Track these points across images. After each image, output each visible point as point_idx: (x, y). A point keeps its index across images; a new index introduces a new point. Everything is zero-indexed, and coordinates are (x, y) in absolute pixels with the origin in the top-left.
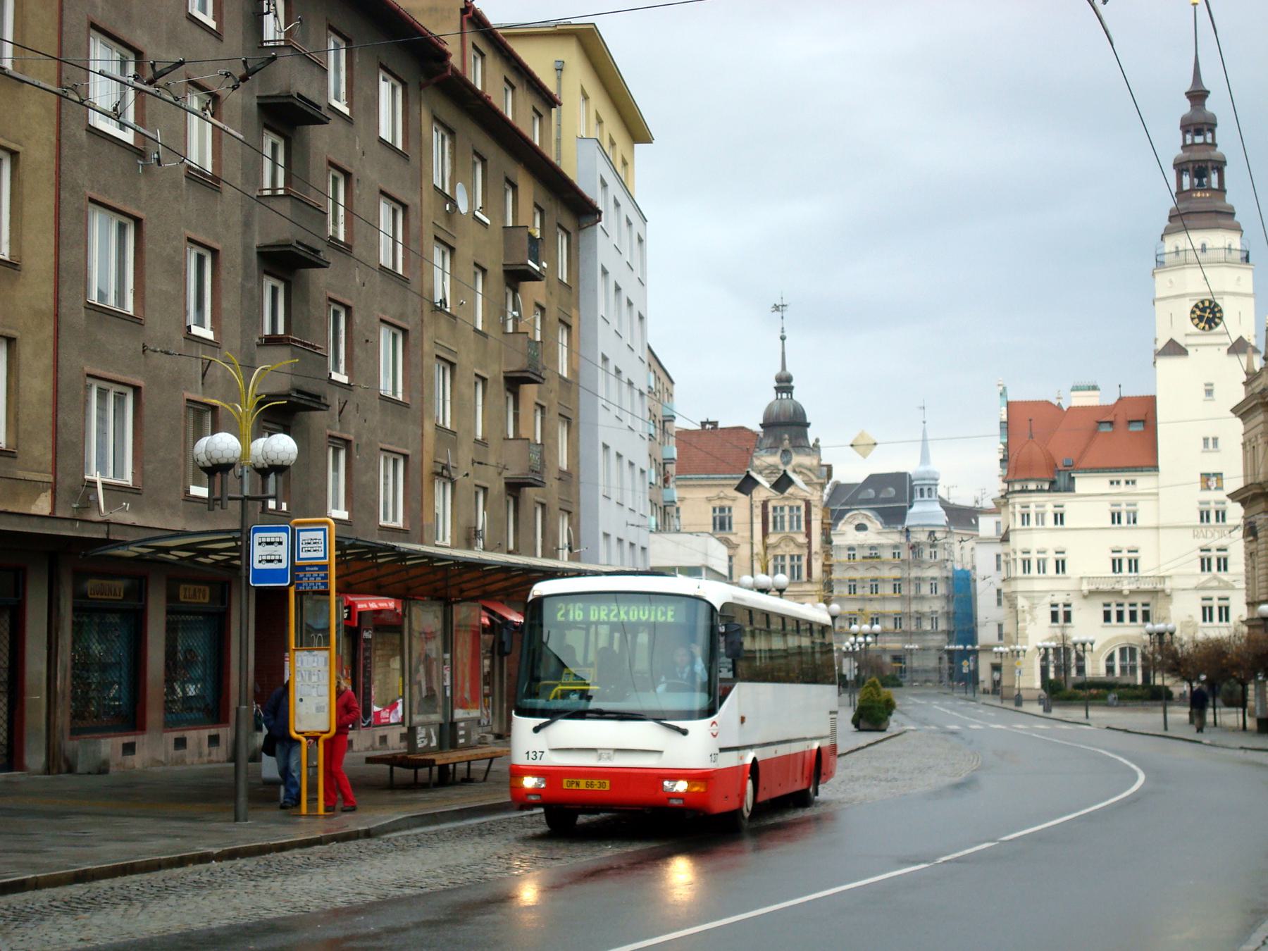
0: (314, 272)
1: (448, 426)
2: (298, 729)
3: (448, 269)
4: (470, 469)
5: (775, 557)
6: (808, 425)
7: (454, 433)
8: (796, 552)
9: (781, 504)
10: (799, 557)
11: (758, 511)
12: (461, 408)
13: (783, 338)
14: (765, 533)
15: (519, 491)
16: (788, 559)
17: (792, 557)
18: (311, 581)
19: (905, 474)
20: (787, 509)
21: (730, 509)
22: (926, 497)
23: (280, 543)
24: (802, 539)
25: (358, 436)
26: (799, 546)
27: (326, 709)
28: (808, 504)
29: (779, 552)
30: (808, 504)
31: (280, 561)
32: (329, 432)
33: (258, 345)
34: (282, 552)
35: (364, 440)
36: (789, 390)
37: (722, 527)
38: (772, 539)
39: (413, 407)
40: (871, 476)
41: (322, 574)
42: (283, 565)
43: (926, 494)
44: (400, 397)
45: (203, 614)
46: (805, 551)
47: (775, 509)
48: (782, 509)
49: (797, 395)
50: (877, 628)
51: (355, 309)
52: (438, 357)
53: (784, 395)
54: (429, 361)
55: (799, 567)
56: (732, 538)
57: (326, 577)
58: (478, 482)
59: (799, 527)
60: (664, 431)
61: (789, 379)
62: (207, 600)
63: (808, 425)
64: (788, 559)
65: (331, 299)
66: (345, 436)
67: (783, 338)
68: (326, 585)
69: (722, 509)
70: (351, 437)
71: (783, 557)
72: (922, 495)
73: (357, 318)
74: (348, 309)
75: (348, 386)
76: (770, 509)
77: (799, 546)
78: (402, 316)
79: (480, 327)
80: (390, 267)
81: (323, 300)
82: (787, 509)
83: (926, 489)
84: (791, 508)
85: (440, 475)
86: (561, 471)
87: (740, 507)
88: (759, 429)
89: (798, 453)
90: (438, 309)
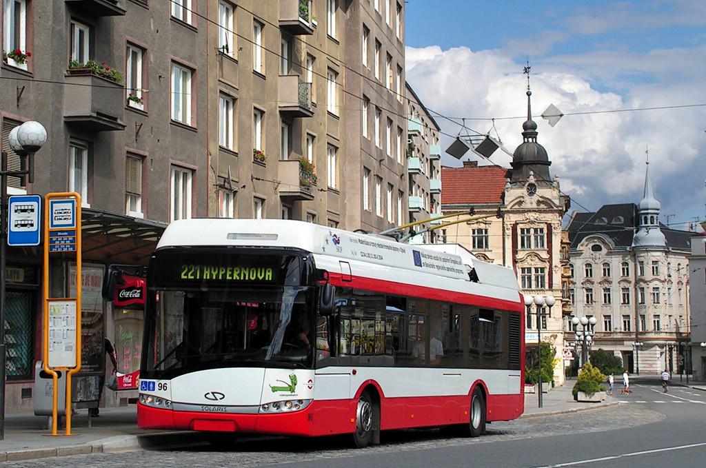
0: (116, 18)
1: (231, 148)
2: (50, 365)
3: (286, 56)
4: (249, 184)
5: (523, 269)
6: (550, 163)
7: (236, 154)
8: (540, 265)
9: (528, 226)
10: (542, 270)
11: (509, 232)
12: (244, 134)
13: (529, 94)
14: (515, 252)
15: (292, 204)
16: (533, 270)
17: (536, 270)
18: (63, 246)
19: (633, 204)
20: (532, 231)
21: (486, 231)
22: (649, 224)
23: (32, 210)
24: (544, 255)
25: (152, 153)
26: (542, 260)
27: (74, 348)
28: (549, 226)
29: (525, 265)
30: (549, 226)
31: (32, 225)
32: (127, 148)
33: (65, 76)
34: (34, 217)
35: (158, 154)
36: (534, 135)
37: (480, 246)
38: (520, 255)
39: (200, 131)
40: (604, 206)
41: (71, 238)
42: (34, 229)
43: (649, 221)
44: (189, 123)
45: (19, 291)
46: (547, 265)
47: (522, 230)
48: (528, 231)
49: (541, 140)
50: (638, 344)
51: (149, 50)
52: (221, 91)
53: (530, 140)
54: (213, 95)
55: (543, 278)
56: (487, 254)
57: (73, 241)
58: (258, 195)
59: (543, 245)
60: (432, 168)
61: (534, 127)
62: (21, 280)
63: (550, 163)
64: (533, 270)
65: (128, 42)
66: (141, 152)
67: (529, 94)
68: (73, 247)
69: (480, 231)
70: (146, 154)
71: (529, 270)
72: (646, 223)
73: (152, 58)
74: (144, 50)
75: (143, 113)
76: (519, 231)
77: (542, 260)
78: (190, 58)
79: (258, 70)
80: (181, 19)
81: (124, 45)
82: (532, 231)
83: (649, 216)
84: (536, 230)
85: (222, 187)
86: (256, 152)
87: (495, 227)
88: (510, 167)
89: (542, 187)
90: (222, 54)
